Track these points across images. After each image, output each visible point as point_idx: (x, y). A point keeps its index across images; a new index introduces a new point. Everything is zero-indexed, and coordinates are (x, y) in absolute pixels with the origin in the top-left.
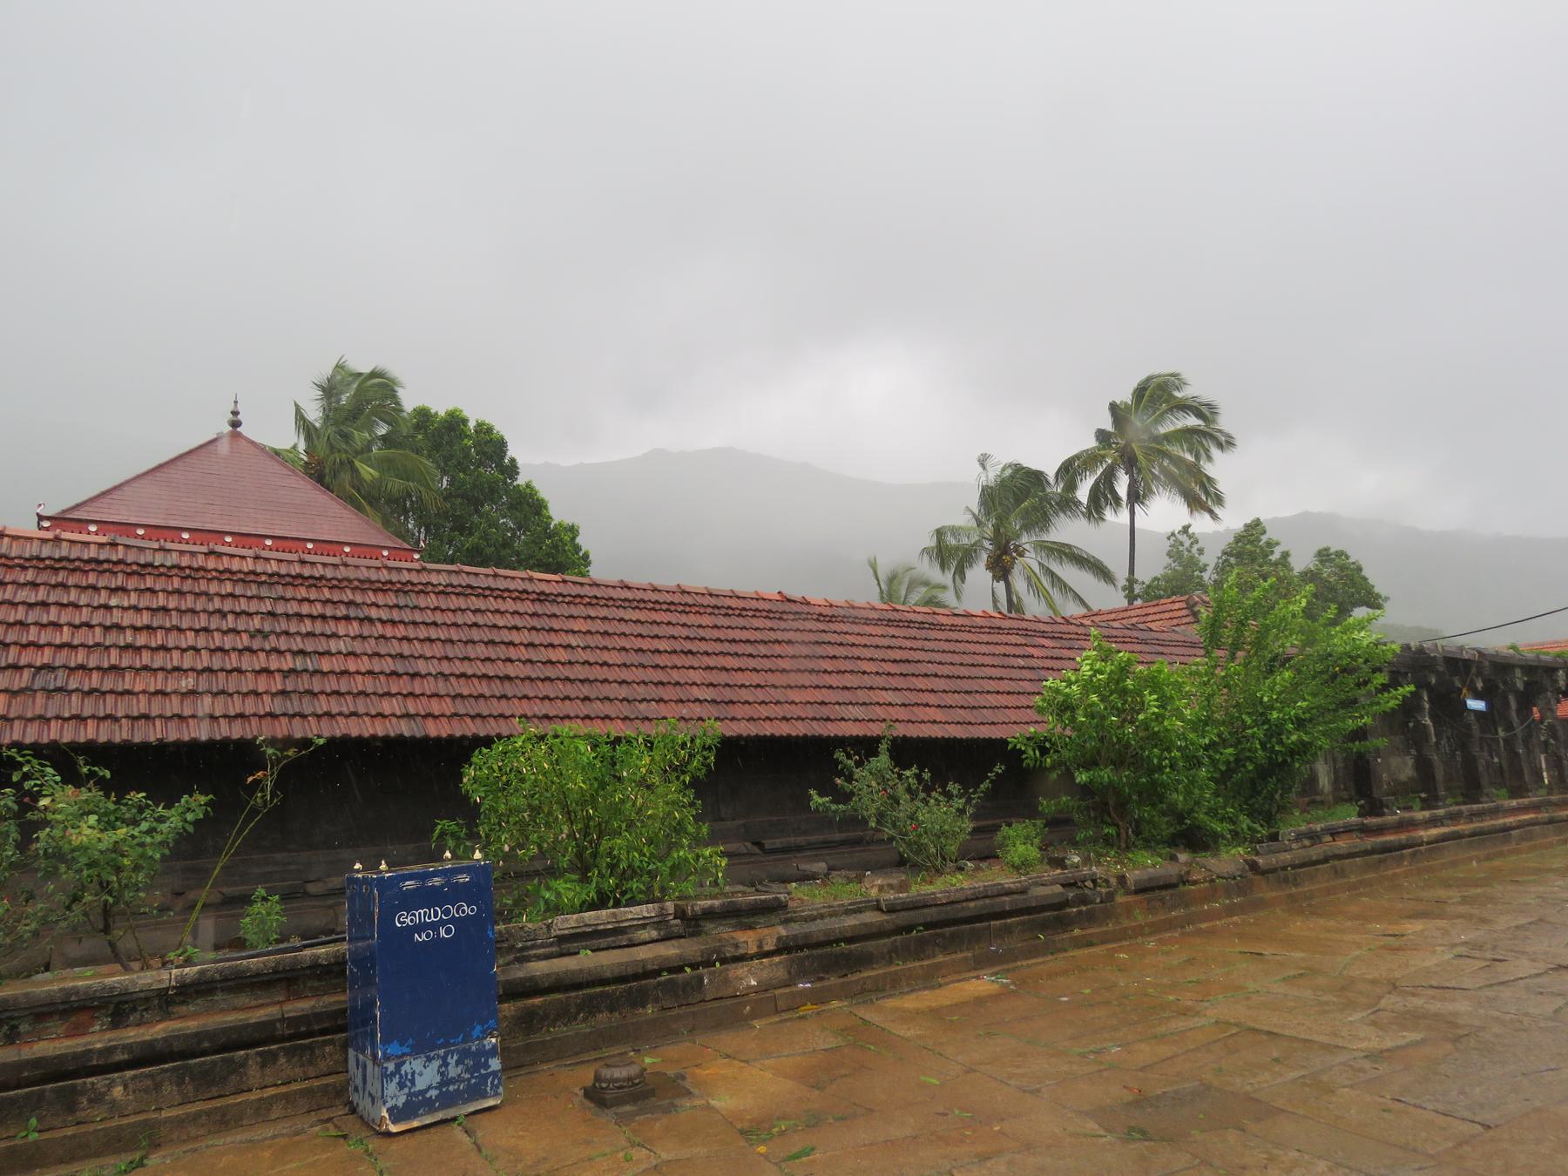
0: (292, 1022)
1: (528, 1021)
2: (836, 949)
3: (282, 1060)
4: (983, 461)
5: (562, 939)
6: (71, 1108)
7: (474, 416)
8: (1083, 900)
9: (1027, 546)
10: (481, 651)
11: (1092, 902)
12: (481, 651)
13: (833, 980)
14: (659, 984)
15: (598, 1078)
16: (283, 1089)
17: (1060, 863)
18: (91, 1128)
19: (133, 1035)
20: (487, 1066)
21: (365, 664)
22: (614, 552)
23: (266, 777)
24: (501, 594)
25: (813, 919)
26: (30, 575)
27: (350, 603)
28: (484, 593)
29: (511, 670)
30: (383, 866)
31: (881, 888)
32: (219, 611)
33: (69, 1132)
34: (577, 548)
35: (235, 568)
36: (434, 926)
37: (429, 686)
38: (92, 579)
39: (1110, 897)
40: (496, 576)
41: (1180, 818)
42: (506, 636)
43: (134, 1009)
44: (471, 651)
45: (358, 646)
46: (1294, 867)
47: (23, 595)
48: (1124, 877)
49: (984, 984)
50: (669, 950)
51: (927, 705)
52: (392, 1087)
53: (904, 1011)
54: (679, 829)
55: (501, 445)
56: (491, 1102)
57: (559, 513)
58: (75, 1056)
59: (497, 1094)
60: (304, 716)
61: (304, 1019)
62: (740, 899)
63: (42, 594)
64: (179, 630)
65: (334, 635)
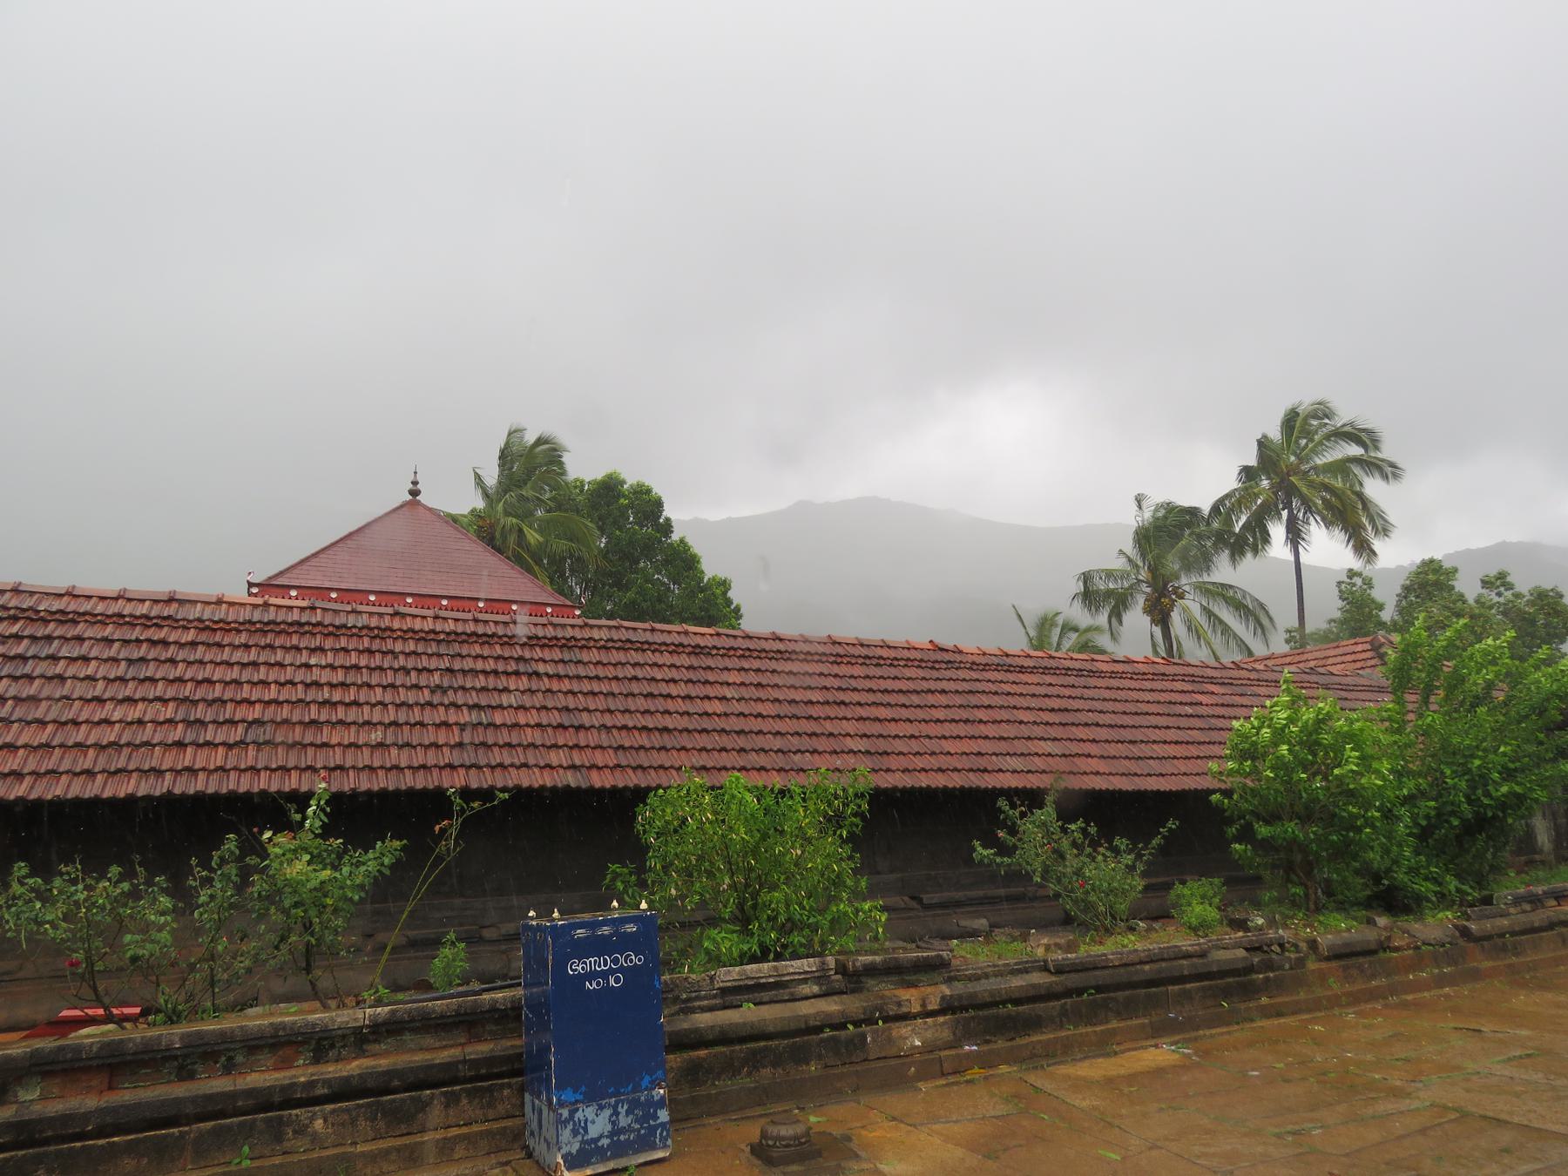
0: (475, 1063)
1: (693, 1073)
2: (1002, 1010)
3: (465, 1101)
4: (1139, 501)
5: (724, 991)
6: (279, 1138)
7: (631, 479)
8: (1268, 966)
9: (1187, 588)
10: (642, 703)
11: (1281, 968)
12: (642, 703)
13: (1001, 1044)
14: (822, 1040)
15: (764, 1135)
16: (465, 1130)
17: (1241, 925)
18: (295, 1158)
19: (332, 1070)
20: (656, 1117)
21: (533, 717)
22: (762, 608)
23: (453, 826)
24: (657, 648)
25: (977, 978)
26: (243, 638)
27: (520, 659)
28: (642, 647)
29: (669, 722)
30: (556, 915)
31: (1048, 948)
32: (403, 668)
33: (277, 1160)
34: (729, 602)
35: (417, 627)
36: (604, 975)
37: (592, 738)
38: (295, 640)
39: (1300, 963)
40: (653, 630)
41: (1377, 878)
42: (664, 689)
43: (332, 1046)
44: (631, 704)
45: (527, 700)
46: (1513, 934)
47: (239, 656)
48: (1315, 941)
49: (1163, 1054)
50: (831, 1006)
51: (1089, 756)
52: (566, 1134)
53: (1082, 1079)
54: (838, 882)
55: (659, 504)
56: (660, 1154)
57: (711, 568)
58: (283, 1088)
59: (665, 1146)
60: (479, 768)
61: (490, 1061)
62: (901, 955)
63: (253, 655)
64: (369, 686)
65: (506, 690)
